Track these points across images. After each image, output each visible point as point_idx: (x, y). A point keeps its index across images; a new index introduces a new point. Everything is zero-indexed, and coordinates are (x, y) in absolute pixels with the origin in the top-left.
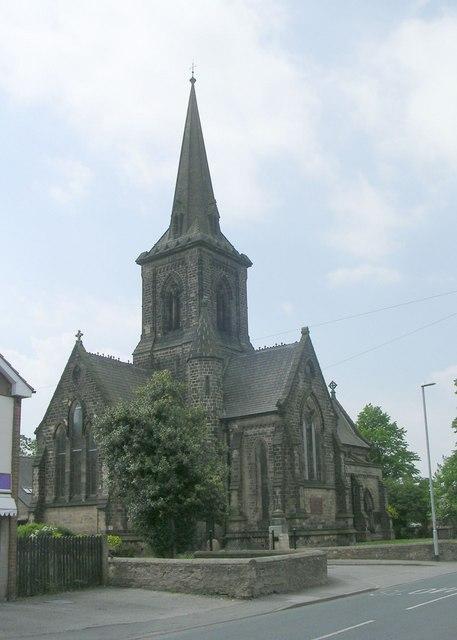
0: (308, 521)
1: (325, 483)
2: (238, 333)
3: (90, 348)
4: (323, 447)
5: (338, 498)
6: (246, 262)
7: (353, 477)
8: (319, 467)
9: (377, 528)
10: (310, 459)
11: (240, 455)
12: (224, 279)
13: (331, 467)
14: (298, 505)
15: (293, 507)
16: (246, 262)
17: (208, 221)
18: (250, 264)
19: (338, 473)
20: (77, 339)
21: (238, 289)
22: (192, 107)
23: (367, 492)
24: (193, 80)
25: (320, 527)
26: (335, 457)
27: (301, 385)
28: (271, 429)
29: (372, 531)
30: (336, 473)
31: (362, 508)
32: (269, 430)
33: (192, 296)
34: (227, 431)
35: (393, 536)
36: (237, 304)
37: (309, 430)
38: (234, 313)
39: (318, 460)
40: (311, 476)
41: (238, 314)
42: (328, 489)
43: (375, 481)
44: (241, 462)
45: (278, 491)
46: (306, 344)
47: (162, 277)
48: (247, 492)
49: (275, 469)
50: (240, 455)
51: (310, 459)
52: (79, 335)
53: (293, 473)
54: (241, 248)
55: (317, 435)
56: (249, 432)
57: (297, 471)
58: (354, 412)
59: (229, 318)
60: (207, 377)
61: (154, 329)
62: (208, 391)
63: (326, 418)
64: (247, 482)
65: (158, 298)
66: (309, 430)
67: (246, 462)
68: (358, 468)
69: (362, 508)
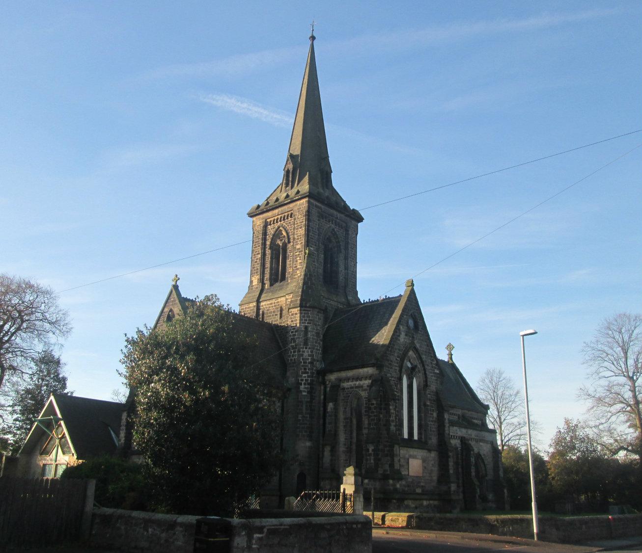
0: (404, 483)
1: (426, 443)
2: (346, 287)
4: (425, 405)
5: (344, 370)
6: (358, 218)
7: (463, 440)
11: (336, 409)
12: (334, 233)
14: (392, 465)
15: (387, 467)
16: (358, 218)
17: (319, 175)
18: (360, 219)
20: (174, 283)
21: (347, 243)
22: (312, 48)
23: (479, 456)
24: (313, 38)
25: (419, 491)
26: (438, 416)
27: (402, 338)
28: (367, 382)
29: (484, 499)
31: (473, 474)
33: (298, 247)
34: (324, 383)
35: (507, 507)
36: (346, 258)
37: (410, 387)
38: (342, 268)
41: (346, 268)
42: (430, 451)
44: (336, 416)
45: (371, 448)
46: (412, 297)
47: (271, 230)
48: (342, 448)
49: (369, 424)
50: (336, 409)
52: (177, 279)
53: (388, 430)
56: (346, 385)
57: (393, 428)
60: (306, 328)
61: (262, 281)
62: (306, 343)
63: (429, 375)
64: (342, 438)
65: (268, 252)
66: (410, 387)
67: (341, 416)
68: (470, 431)
69: (473, 474)
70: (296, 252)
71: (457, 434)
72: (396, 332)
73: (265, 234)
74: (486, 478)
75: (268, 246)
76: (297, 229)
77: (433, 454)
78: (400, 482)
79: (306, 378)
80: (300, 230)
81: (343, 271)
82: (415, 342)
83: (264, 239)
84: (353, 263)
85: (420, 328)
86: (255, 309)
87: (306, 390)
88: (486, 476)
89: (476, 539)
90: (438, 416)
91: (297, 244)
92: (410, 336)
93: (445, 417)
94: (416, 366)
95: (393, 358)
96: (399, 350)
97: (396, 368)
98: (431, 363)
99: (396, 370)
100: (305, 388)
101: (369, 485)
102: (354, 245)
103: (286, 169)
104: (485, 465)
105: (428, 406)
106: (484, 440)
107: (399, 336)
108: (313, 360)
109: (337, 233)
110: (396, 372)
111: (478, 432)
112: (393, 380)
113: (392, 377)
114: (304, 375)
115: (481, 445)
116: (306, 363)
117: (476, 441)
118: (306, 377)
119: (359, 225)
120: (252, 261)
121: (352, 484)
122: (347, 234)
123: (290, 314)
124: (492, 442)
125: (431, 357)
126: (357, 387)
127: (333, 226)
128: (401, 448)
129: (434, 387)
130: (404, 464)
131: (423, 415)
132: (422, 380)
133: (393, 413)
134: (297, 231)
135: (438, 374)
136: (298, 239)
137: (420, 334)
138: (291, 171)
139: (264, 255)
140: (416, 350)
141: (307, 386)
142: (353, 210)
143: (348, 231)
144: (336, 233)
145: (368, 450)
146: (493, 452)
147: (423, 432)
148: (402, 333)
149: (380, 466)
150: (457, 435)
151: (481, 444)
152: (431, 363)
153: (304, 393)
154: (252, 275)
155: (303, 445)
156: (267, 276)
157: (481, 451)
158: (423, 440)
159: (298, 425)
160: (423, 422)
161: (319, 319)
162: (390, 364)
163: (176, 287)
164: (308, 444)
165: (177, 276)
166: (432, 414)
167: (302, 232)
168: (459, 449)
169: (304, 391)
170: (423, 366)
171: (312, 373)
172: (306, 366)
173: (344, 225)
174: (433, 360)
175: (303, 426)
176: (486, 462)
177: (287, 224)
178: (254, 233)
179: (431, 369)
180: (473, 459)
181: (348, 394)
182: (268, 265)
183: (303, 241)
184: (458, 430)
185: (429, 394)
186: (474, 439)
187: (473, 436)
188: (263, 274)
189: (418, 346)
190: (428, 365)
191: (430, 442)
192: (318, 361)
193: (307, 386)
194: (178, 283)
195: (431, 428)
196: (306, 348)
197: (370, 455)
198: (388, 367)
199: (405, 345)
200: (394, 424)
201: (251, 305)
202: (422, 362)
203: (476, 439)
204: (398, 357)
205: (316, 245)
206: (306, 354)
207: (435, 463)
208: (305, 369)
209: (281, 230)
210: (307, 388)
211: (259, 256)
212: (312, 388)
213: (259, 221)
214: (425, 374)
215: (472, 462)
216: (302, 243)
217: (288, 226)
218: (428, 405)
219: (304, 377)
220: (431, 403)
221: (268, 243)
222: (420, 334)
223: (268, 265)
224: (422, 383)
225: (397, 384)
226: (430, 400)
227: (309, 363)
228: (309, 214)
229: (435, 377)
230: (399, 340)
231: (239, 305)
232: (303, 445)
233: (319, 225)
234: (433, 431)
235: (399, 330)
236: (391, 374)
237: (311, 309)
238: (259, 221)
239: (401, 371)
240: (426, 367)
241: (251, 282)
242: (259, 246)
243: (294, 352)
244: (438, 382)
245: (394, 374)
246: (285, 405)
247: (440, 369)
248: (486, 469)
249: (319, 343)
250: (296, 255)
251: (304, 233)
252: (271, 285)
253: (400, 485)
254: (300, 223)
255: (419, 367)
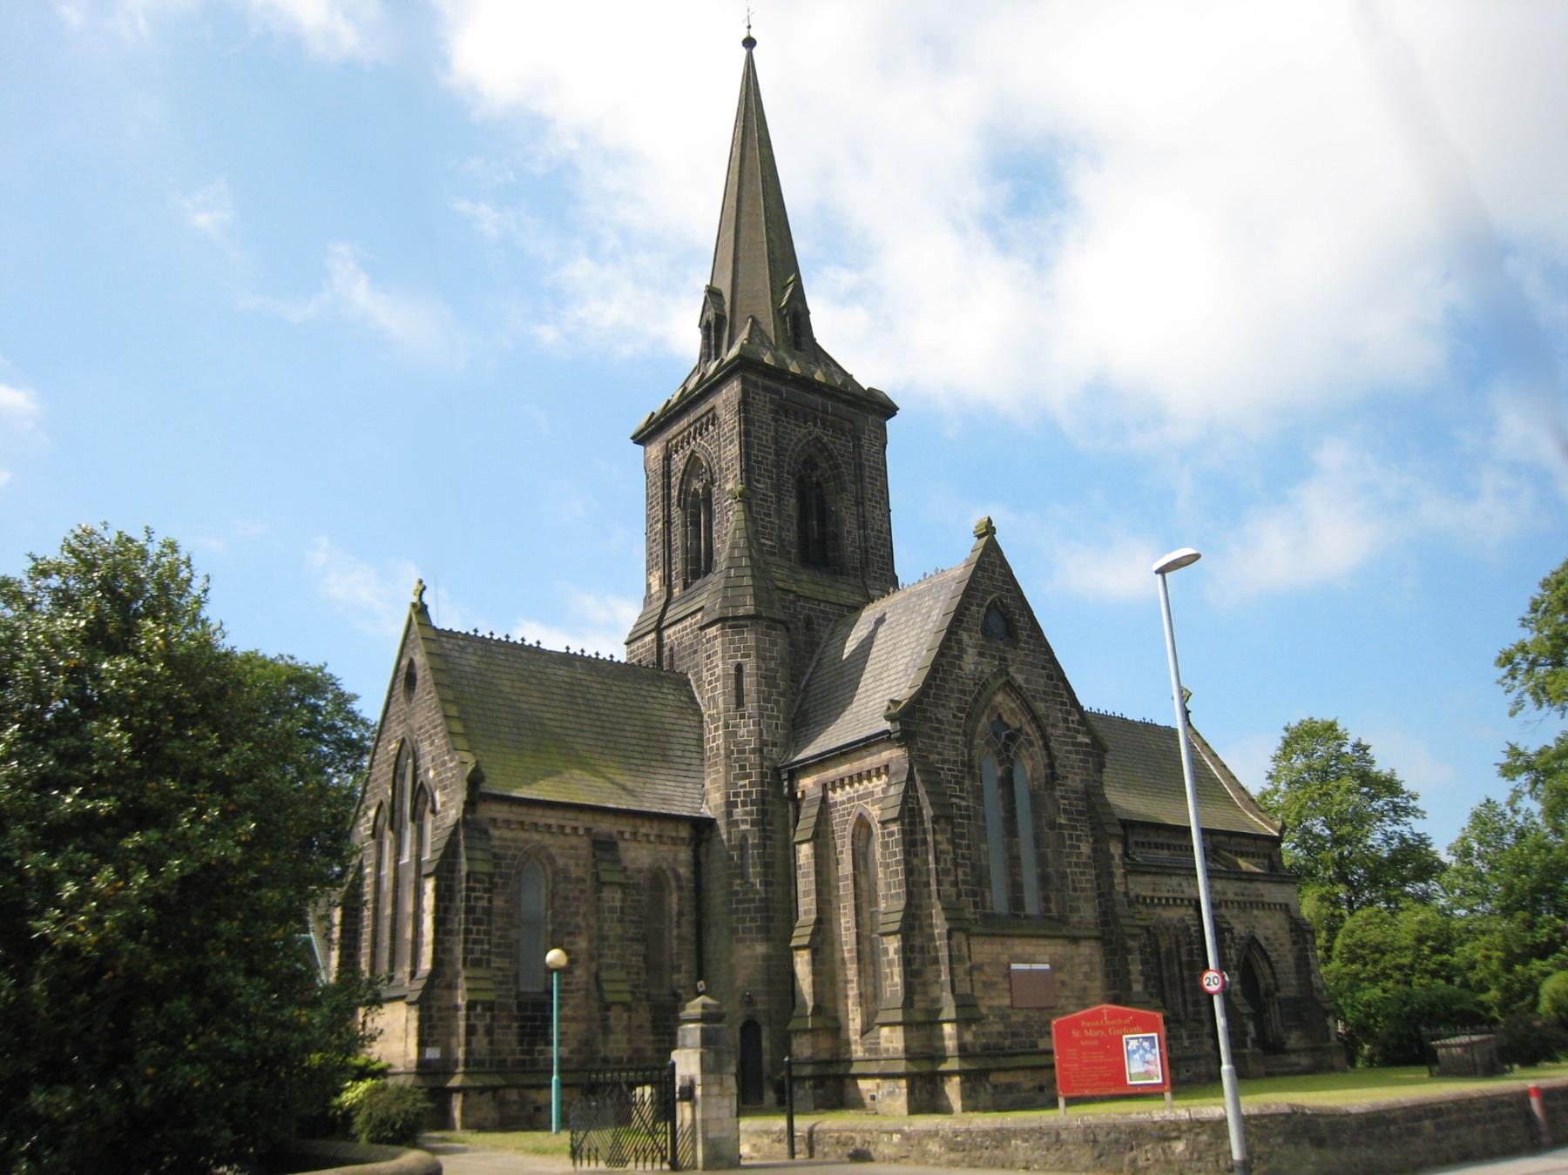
1: (1062, 920)
3: (445, 617)
4: (1053, 825)
5: (1108, 963)
8: (1044, 880)
9: (1294, 1040)
10: (1013, 861)
13: (1086, 880)
19: (1104, 894)
20: (415, 599)
24: (749, 43)
30: (1101, 896)
32: (878, 784)
36: (859, 503)
38: (850, 525)
39: (1042, 861)
40: (1016, 902)
42: (1075, 940)
43: (1280, 917)
47: (679, 462)
51: (1013, 861)
54: (867, 373)
55: (1034, 796)
58: (866, 388)
59: (836, 537)
61: (667, 581)
65: (676, 512)
66: (1007, 782)
70: (726, 501)
71: (1183, 892)
72: (950, 648)
73: (667, 474)
74: (1278, 994)
75: (674, 501)
76: (725, 446)
77: (1088, 951)
78: (974, 1028)
79: (748, 789)
80: (730, 447)
81: (855, 532)
82: (1011, 670)
83: (667, 486)
84: (878, 512)
85: (1023, 635)
86: (655, 645)
87: (749, 818)
88: (1278, 989)
89: (1554, 1077)
90: (1094, 850)
91: (726, 482)
92: (993, 657)
93: (1112, 850)
94: (1020, 730)
95: (944, 714)
96: (963, 692)
97: (957, 738)
98: (1065, 720)
99: (957, 742)
100: (746, 813)
101: (892, 1042)
102: (880, 470)
103: (704, 323)
104: (1270, 965)
105: (1061, 826)
106: (1263, 904)
107: (959, 657)
108: (763, 744)
109: (831, 446)
110: (956, 749)
111: (1243, 884)
112: (949, 770)
113: (944, 761)
114: (741, 783)
115: (1256, 917)
116: (743, 752)
117: (1240, 907)
118: (745, 786)
119: (890, 424)
120: (648, 539)
121: (696, 1048)
122: (859, 446)
123: (704, 640)
124: (1287, 906)
125: (1063, 704)
126: (860, 797)
127: (817, 431)
128: (973, 940)
129: (1078, 778)
130: (994, 979)
131: (1049, 851)
132: (1042, 763)
133: (947, 853)
134: (725, 453)
135: (1087, 745)
136: (728, 469)
137: (1024, 649)
138: (713, 325)
139: (668, 522)
140: (1010, 686)
141: (748, 808)
142: (870, 389)
143: (859, 439)
144: (825, 446)
145: (886, 951)
146: (1292, 930)
147: (1053, 895)
148: (969, 649)
149: (919, 989)
150: (1182, 896)
151: (1256, 912)
152: (1065, 720)
153: (743, 827)
154: (649, 573)
155: (747, 952)
156: (678, 566)
157: (1256, 931)
158: (1054, 913)
159: (734, 906)
160: (1051, 870)
161: (773, 643)
162: (938, 730)
163: (420, 610)
164: (761, 949)
165: (421, 582)
166: (1079, 848)
167: (733, 450)
168: (1193, 929)
169: (744, 822)
170: (1040, 728)
171: (763, 775)
172: (745, 760)
173: (848, 426)
174: (1069, 713)
175: (746, 905)
176: (1274, 956)
177: (706, 442)
178: (647, 478)
179: (1065, 736)
180: (1233, 951)
181: (843, 815)
182: (677, 541)
183: (738, 472)
184: (1185, 884)
185: (1063, 798)
186: (1232, 902)
187: (1230, 896)
188: (668, 562)
189: (1020, 679)
190: (1054, 726)
191: (1075, 918)
192: (775, 745)
193: (748, 808)
194: (426, 599)
195: (1073, 881)
196: (742, 717)
197: (890, 963)
198: (930, 737)
199: (980, 679)
200: (952, 878)
201: (648, 638)
202: (1035, 718)
203: (1238, 903)
204: (961, 710)
205: (770, 478)
206: (743, 731)
207: (1092, 970)
208: (742, 768)
209: (698, 458)
210: (751, 813)
211: (660, 525)
212: (763, 813)
213: (656, 449)
214: (1047, 747)
215: (1231, 960)
216: (736, 475)
217: (710, 445)
218: (1060, 824)
219: (742, 787)
220: (1069, 820)
221: (675, 493)
222: (1024, 649)
223: (677, 541)
224: (1043, 772)
225: (963, 778)
226: (1065, 811)
227: (753, 751)
228: (745, 404)
229: (1077, 753)
230: (960, 668)
231: (627, 643)
232: (747, 952)
233: (776, 431)
234: (1083, 890)
235: (959, 642)
236: (939, 754)
237: (749, 623)
238: (656, 449)
239: (969, 744)
240: (1050, 730)
241: (649, 586)
242: (658, 504)
243: (716, 729)
244: (1090, 765)
245: (950, 754)
246: (703, 860)
247: (1090, 732)
248: (1274, 974)
249: (777, 702)
250: (726, 507)
251: (738, 452)
252: (686, 586)
253: (976, 1035)
254: (730, 431)
255: (1030, 732)
